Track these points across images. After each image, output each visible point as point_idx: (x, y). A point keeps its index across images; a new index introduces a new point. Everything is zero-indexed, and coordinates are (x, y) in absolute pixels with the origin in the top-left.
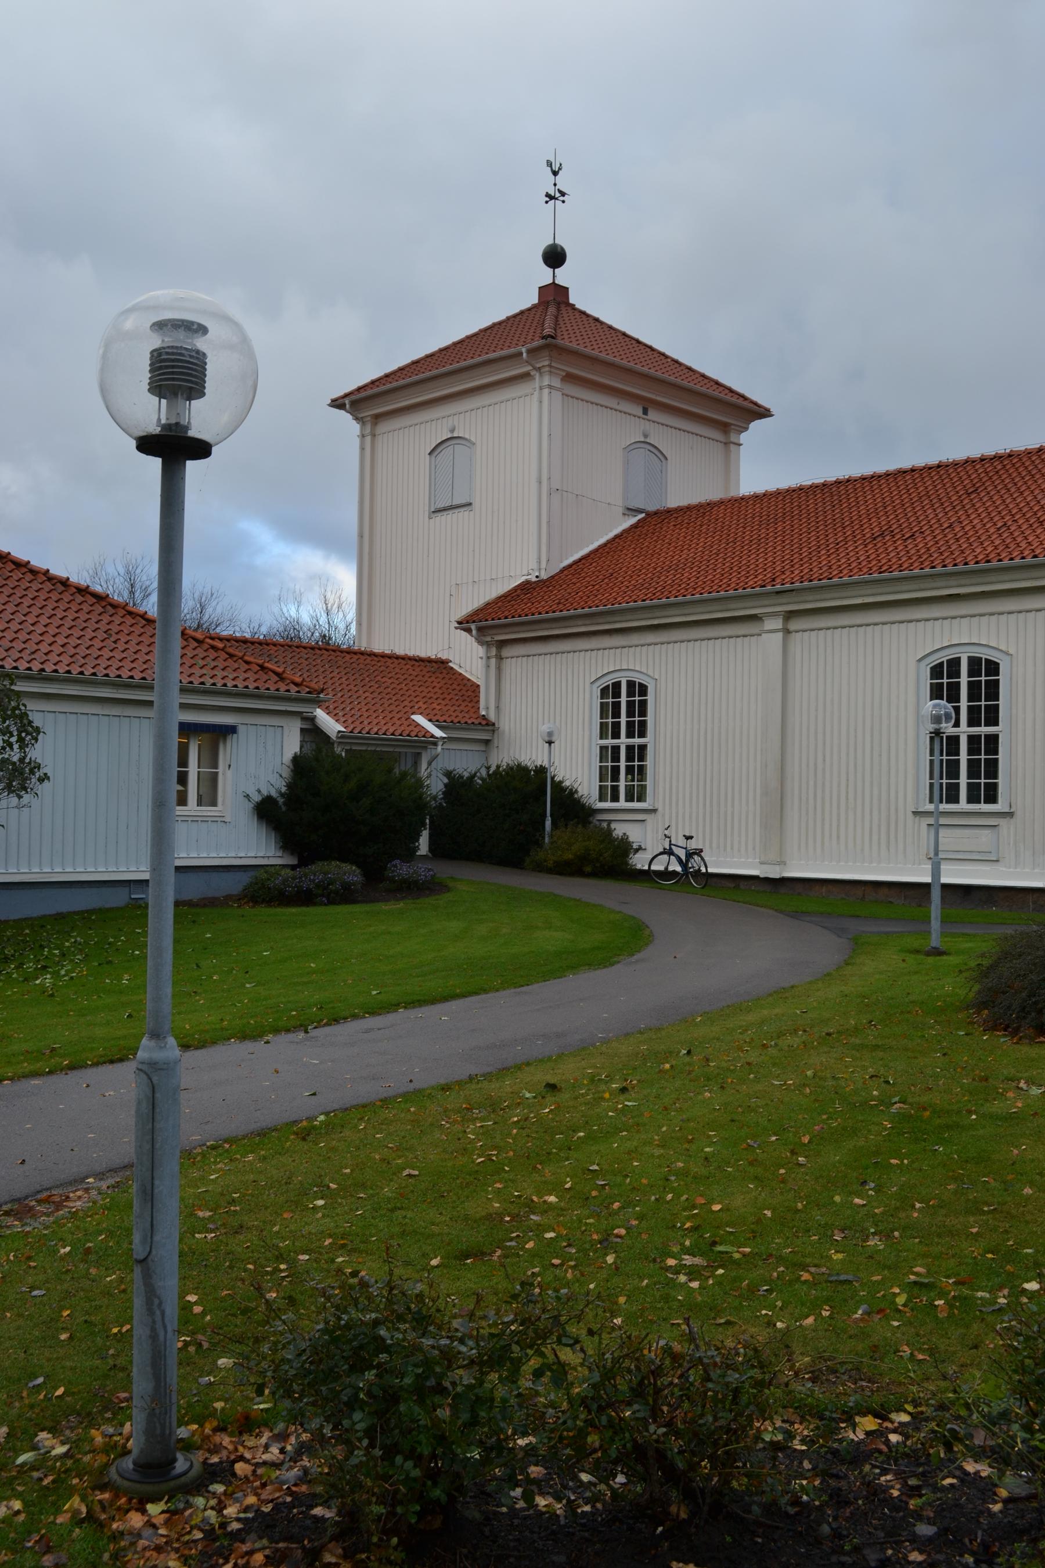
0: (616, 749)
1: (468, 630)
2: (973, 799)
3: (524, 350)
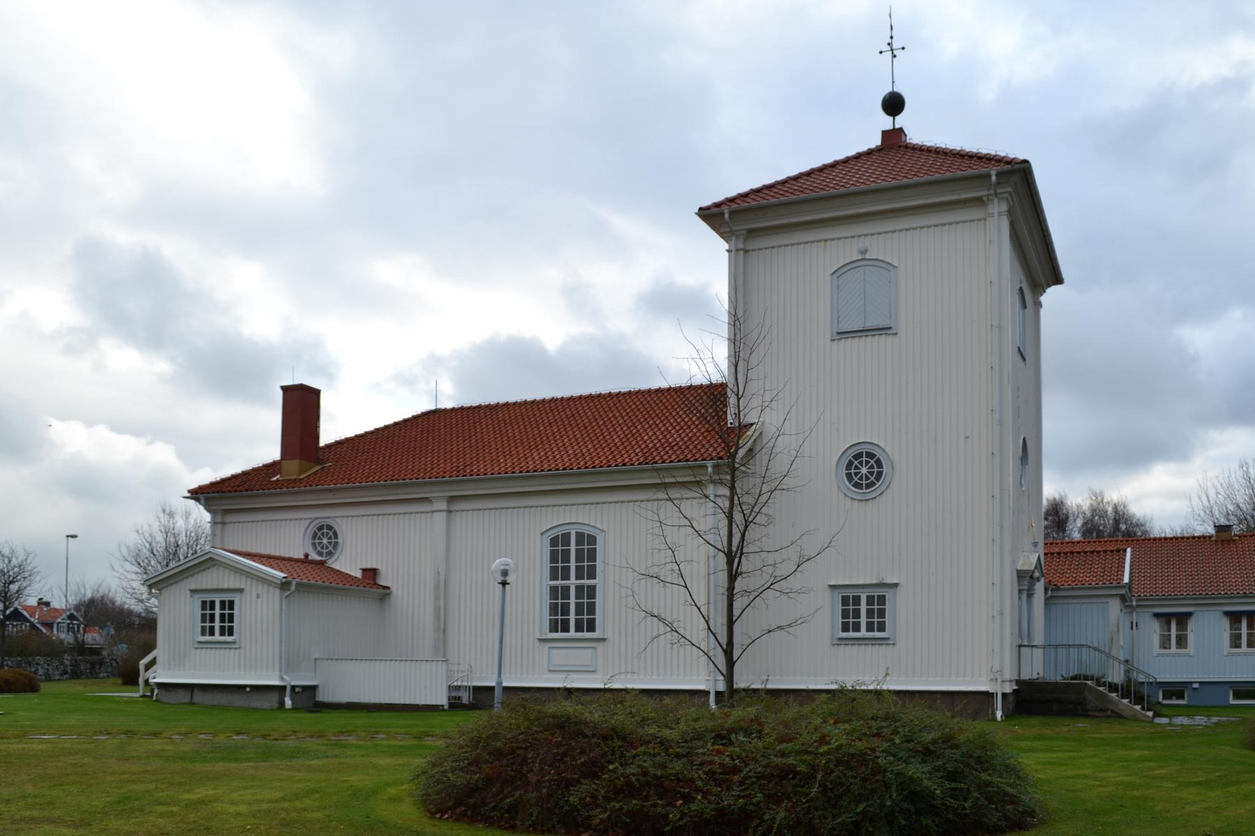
0: (566, 589)
1: (197, 500)
2: (222, 634)
3: (993, 173)
